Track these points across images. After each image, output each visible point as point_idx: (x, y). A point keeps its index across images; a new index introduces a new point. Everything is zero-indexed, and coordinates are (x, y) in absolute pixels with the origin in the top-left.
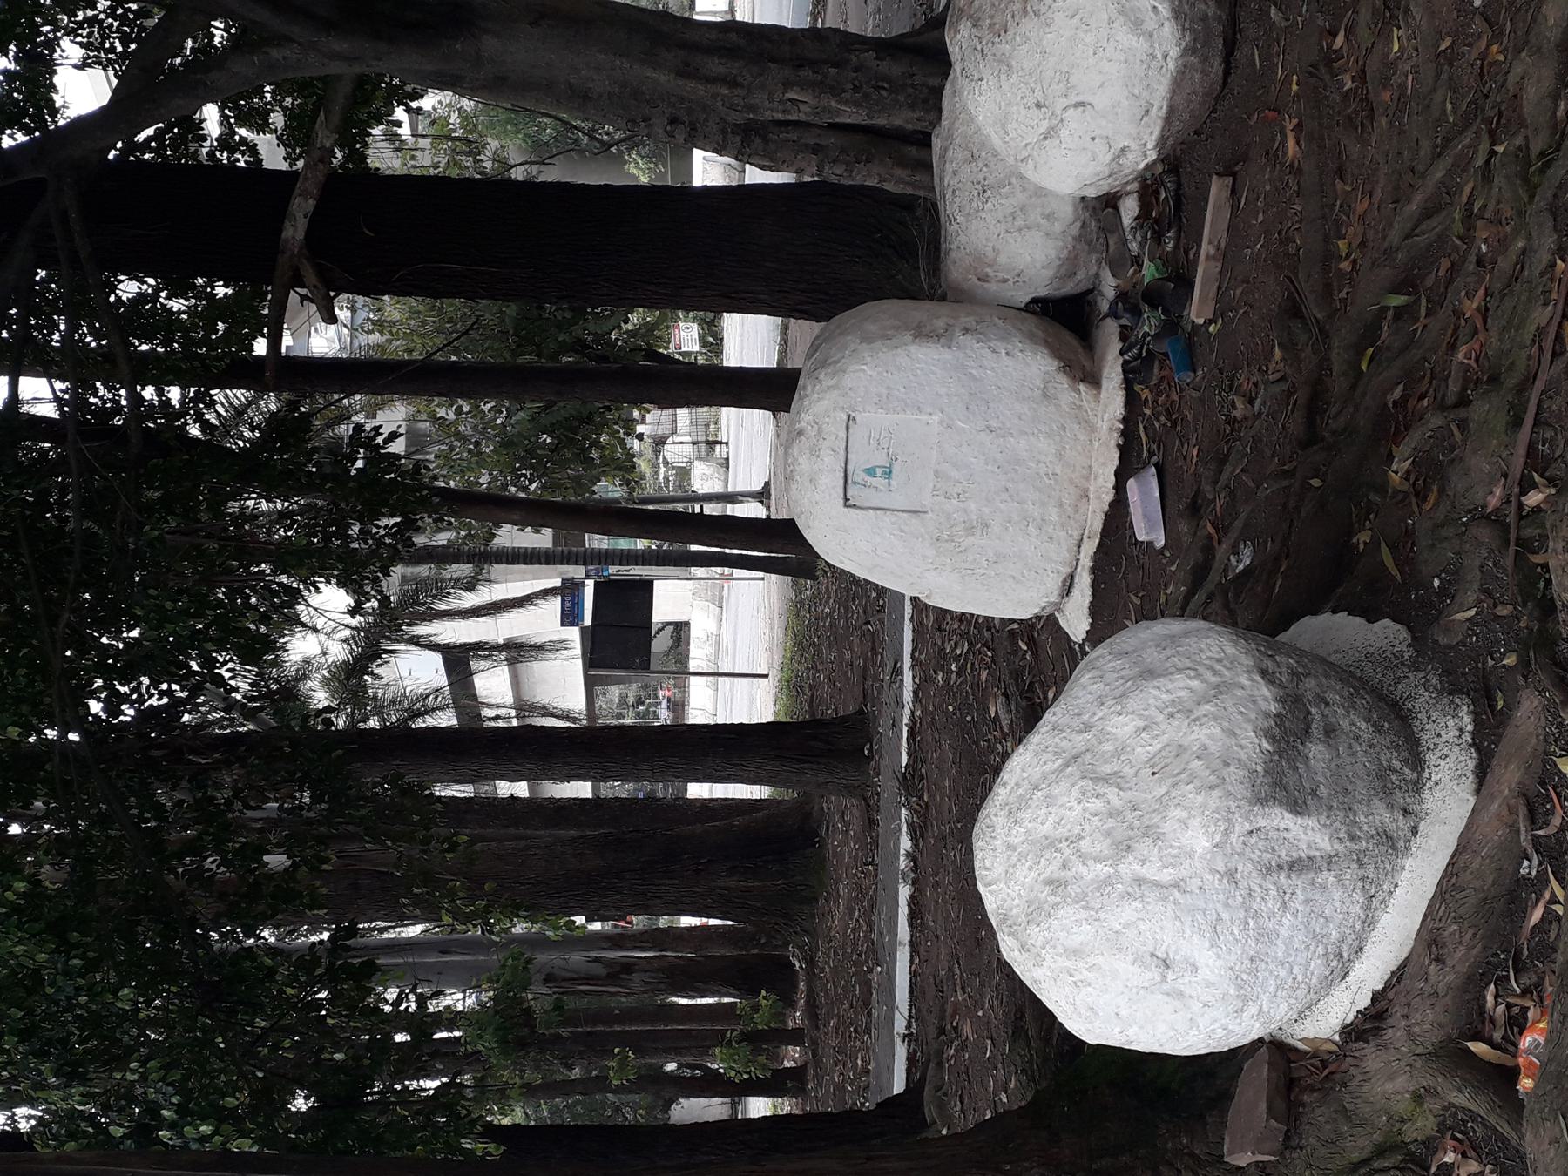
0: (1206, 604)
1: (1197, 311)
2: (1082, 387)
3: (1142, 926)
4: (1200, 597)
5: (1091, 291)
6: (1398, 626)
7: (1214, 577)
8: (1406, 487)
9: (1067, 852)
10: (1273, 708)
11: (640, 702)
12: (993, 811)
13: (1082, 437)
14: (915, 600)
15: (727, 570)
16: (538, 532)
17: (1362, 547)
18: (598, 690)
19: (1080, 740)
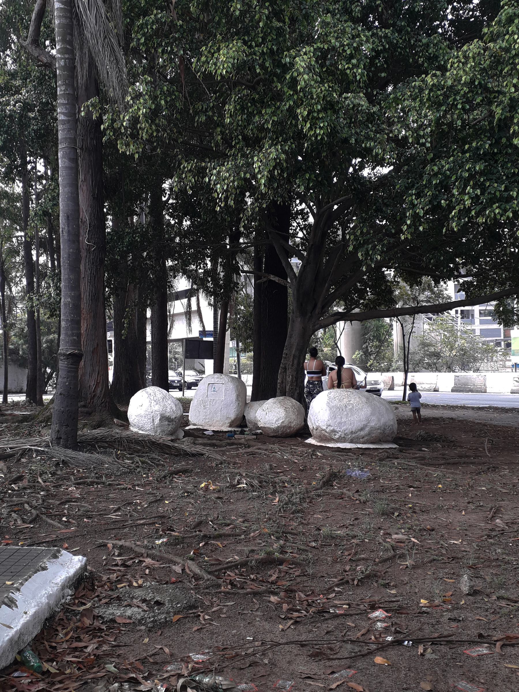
18: (180, 344)
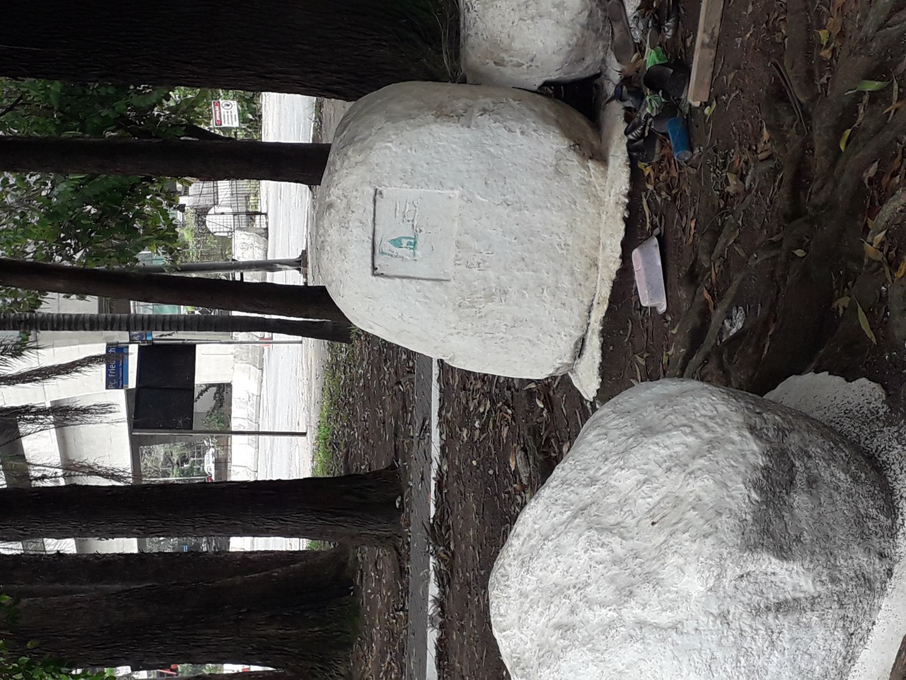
0: (703, 365)
1: (694, 95)
2: (591, 164)
3: (643, 666)
4: (697, 359)
5: (598, 76)
6: (873, 385)
7: (710, 339)
8: (880, 256)
9: (575, 598)
10: (761, 461)
11: (184, 460)
12: (507, 561)
13: (592, 210)
14: (441, 362)
15: (267, 335)
16: (83, 298)
17: (841, 311)
18: (144, 449)
19: (586, 494)
